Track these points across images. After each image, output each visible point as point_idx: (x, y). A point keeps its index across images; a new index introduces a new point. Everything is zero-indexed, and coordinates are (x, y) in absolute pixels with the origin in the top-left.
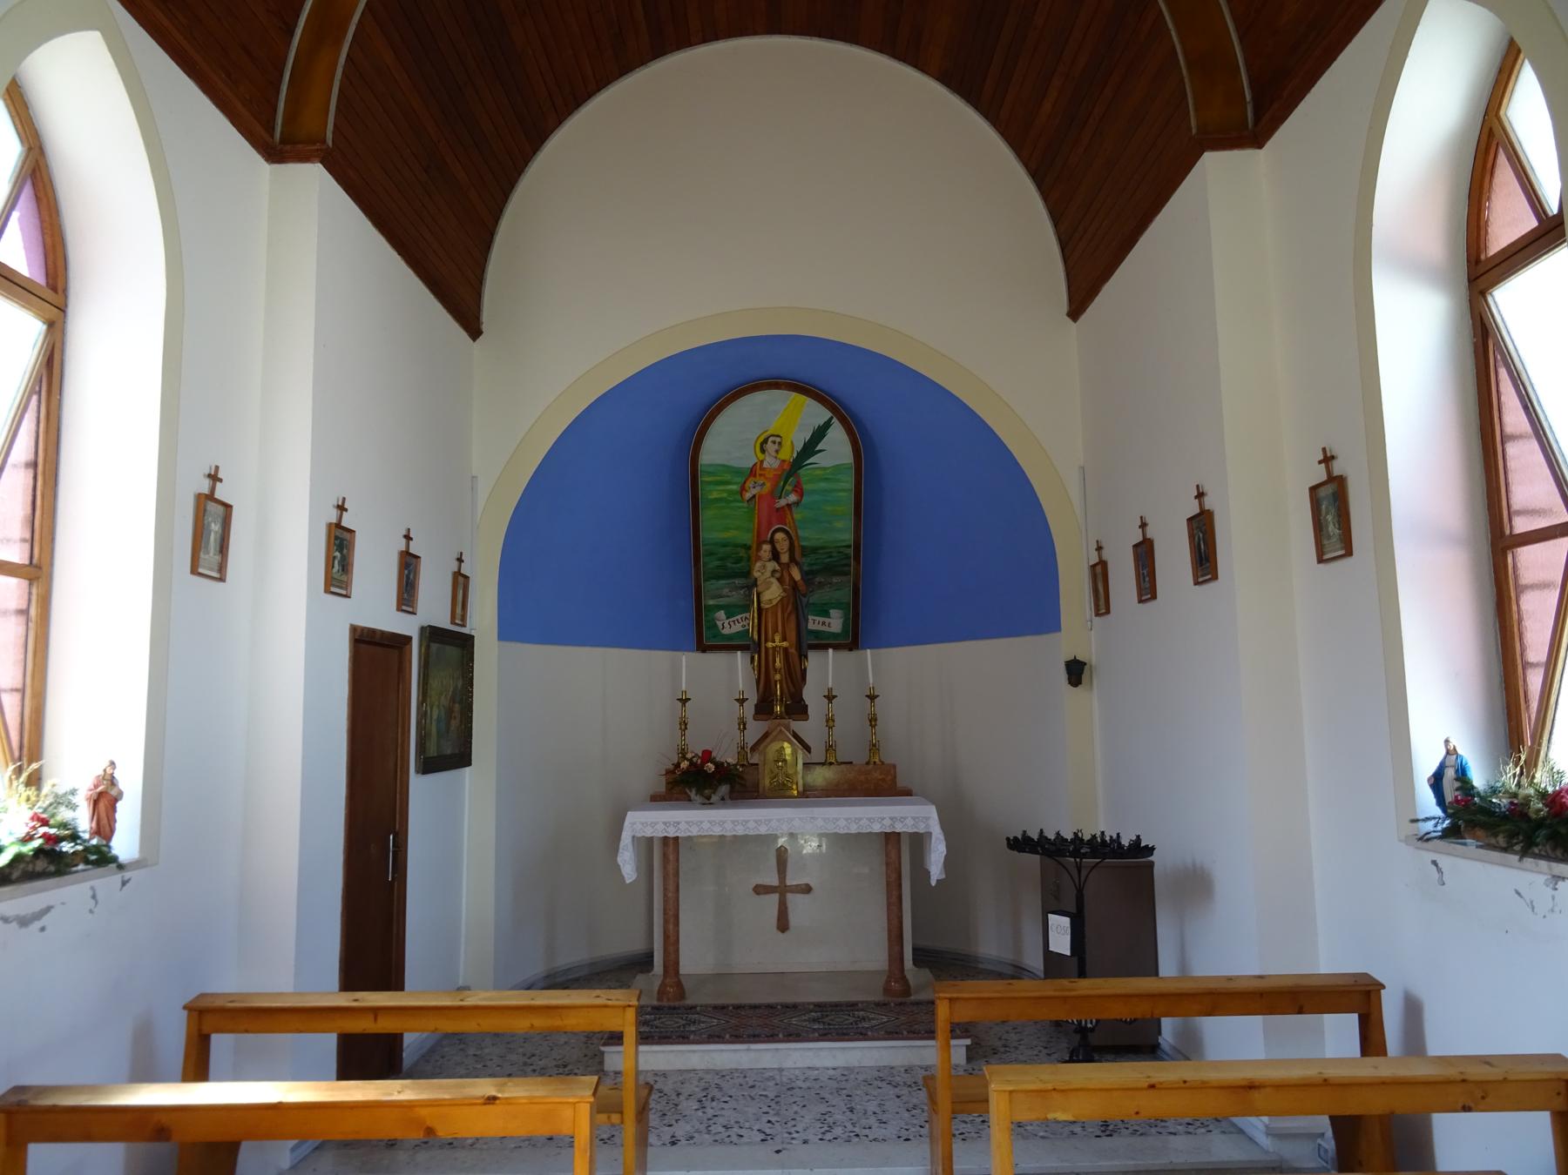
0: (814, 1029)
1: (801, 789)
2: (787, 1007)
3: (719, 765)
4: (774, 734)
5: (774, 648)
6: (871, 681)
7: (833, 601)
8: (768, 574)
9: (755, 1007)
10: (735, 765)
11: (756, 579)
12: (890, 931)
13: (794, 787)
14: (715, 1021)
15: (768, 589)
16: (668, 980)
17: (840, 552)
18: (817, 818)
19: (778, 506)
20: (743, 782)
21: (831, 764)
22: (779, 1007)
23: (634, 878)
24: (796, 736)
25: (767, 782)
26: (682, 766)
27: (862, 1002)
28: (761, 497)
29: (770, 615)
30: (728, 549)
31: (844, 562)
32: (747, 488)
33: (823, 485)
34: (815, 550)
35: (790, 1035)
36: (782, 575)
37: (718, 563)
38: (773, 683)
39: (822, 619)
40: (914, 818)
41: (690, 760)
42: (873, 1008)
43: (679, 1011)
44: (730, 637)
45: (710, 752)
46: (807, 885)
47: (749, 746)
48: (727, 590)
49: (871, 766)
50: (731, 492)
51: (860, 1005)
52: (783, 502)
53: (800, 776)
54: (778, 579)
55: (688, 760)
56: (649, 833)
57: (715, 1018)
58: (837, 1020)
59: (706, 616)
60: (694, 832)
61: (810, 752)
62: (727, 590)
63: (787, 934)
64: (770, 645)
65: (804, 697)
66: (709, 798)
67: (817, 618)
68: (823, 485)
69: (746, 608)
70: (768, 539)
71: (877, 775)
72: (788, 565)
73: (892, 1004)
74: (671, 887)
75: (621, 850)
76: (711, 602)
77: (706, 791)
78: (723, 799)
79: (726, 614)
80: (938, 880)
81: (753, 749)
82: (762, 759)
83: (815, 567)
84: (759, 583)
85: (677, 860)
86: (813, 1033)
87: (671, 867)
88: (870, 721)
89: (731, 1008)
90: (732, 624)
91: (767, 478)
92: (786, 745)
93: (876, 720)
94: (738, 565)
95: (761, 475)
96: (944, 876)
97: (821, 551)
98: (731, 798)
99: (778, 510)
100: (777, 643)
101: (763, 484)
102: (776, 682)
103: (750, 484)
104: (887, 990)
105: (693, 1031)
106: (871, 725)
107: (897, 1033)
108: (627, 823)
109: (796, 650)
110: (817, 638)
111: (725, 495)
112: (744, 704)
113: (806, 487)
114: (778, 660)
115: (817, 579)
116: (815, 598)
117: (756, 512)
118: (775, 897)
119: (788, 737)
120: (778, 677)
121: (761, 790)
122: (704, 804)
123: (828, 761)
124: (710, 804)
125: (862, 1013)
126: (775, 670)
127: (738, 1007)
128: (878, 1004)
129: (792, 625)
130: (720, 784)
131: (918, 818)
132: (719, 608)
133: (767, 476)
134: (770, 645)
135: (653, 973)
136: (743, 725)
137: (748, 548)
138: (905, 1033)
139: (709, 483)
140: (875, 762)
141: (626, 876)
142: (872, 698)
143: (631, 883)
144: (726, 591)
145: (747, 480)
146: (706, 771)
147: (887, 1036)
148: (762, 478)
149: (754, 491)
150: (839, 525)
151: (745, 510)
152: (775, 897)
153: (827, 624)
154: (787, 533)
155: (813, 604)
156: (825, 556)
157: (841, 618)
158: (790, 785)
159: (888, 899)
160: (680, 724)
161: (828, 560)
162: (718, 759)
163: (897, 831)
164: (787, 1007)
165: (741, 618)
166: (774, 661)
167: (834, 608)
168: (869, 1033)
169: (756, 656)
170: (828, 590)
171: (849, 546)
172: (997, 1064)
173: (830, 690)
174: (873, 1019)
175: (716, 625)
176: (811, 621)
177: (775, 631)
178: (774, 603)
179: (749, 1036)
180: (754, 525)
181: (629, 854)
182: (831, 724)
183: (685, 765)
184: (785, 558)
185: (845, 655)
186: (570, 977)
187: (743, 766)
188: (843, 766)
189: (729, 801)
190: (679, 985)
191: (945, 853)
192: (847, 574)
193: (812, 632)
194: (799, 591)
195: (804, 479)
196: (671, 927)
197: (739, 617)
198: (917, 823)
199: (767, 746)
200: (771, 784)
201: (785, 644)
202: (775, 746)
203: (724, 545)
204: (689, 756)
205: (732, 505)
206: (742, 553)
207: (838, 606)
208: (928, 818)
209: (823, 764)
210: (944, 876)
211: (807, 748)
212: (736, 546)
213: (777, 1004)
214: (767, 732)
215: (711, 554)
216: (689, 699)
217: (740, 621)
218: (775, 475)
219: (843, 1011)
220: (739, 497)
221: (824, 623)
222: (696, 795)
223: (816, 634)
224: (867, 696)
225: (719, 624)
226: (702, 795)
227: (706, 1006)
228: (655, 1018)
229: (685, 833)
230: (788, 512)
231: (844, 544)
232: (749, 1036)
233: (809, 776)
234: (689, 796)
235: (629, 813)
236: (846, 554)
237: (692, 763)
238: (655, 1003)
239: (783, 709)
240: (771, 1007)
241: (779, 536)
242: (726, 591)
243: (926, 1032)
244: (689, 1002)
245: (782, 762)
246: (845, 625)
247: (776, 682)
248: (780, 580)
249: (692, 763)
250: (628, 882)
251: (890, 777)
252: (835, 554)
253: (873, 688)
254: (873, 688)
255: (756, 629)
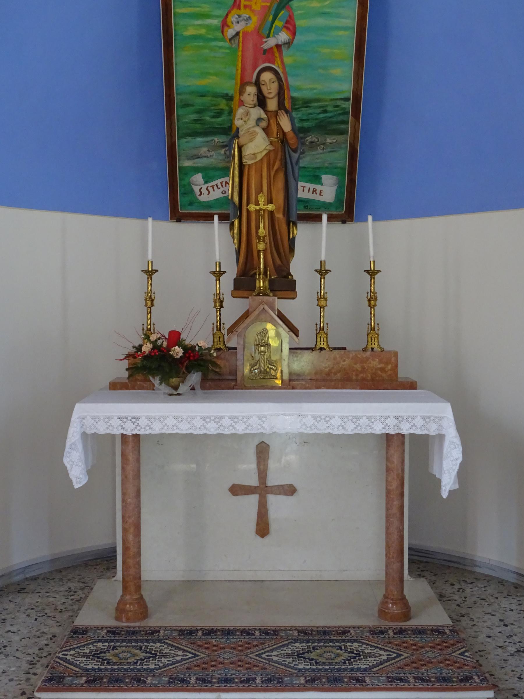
0: (300, 670)
1: (286, 377)
2: (267, 633)
3: (189, 350)
4: (256, 313)
5: (258, 212)
6: (372, 253)
7: (326, 165)
8: (252, 122)
9: (228, 632)
10: (209, 349)
11: (238, 129)
12: (388, 546)
13: (279, 375)
14: (180, 653)
15: (251, 141)
16: (128, 597)
17: (337, 106)
18: (307, 416)
19: (265, 46)
20: (217, 370)
21: (321, 349)
22: (257, 633)
23: (83, 483)
24: (281, 316)
25: (247, 371)
26: (144, 349)
27: (354, 628)
28: (245, 34)
29: (253, 173)
30: (206, 100)
31: (341, 118)
32: (229, 24)
33: (320, 21)
34: (307, 103)
35: (270, 680)
36: (269, 124)
37: (194, 116)
38: (255, 254)
39: (312, 186)
40: (423, 418)
41: (154, 343)
42: (368, 639)
43: (139, 637)
44: (208, 205)
45: (179, 334)
46: (291, 486)
47: (227, 327)
48: (205, 149)
49: (368, 353)
50: (208, 27)
51: (352, 632)
52: (271, 42)
53: (285, 363)
54: (264, 129)
55: (151, 342)
56: (102, 429)
57: (180, 649)
58: (327, 655)
59: (180, 180)
60: (157, 429)
61: (297, 336)
62: (205, 149)
63: (267, 539)
64: (253, 207)
65: (292, 271)
66: (176, 388)
67: (308, 185)
68: (320, 21)
69: (225, 171)
70: (254, 80)
71: (375, 363)
72: (276, 114)
73: (391, 632)
74: (131, 491)
75: (67, 449)
76: (187, 164)
77: (174, 380)
78: (193, 389)
79: (203, 178)
80: (450, 491)
81: (231, 330)
82: (242, 342)
83: (306, 125)
84: (241, 133)
85: (138, 460)
86: (298, 677)
87: (130, 468)
88: (369, 300)
89: (200, 633)
90: (210, 189)
91: (253, 11)
92: (269, 326)
93: (376, 299)
94: (219, 120)
95: (245, 7)
96: (457, 487)
97: (316, 104)
98: (203, 388)
99: (265, 51)
100: (261, 206)
101: (249, 18)
102: (259, 252)
103: (232, 18)
104: (382, 613)
105: (152, 670)
106: (369, 306)
107: (401, 680)
108: (75, 417)
109: (284, 215)
110: (306, 207)
111: (203, 31)
112: (153, 277)
113: (300, 23)
114: (261, 226)
115: (309, 139)
116: (306, 161)
117: (240, 53)
118: (254, 499)
119: (272, 318)
120: (261, 246)
121: (239, 378)
122: (170, 395)
123: (318, 346)
124: (179, 394)
125: (356, 644)
126: (259, 238)
127: (209, 632)
128: (373, 632)
129: (280, 184)
130: (189, 372)
131: (429, 417)
132: (196, 170)
133: (254, 7)
134: (253, 207)
135: (115, 578)
136: (219, 303)
137: (229, 98)
138: (412, 680)
139: (185, 15)
140: (372, 349)
141: (74, 480)
142: (372, 273)
143: (79, 488)
144: (204, 150)
145: (229, 12)
146: (172, 356)
147: (389, 685)
148: (248, 10)
149: (238, 28)
150: (337, 72)
151: (227, 51)
152: (254, 499)
153: (318, 192)
154: (276, 73)
155: (304, 168)
156: (319, 111)
157: (334, 185)
158: (273, 373)
159: (387, 509)
160: (146, 300)
161: (322, 116)
162: (187, 342)
163: (402, 432)
164: (267, 633)
165: (221, 183)
166: (258, 228)
167: (326, 173)
168: (367, 679)
169: (236, 222)
170: (321, 151)
171: (347, 99)
172: (187, 107)
173: (323, 263)
174: (370, 655)
175: (192, 191)
176: (300, 189)
177: (260, 190)
178: (259, 158)
179: (220, 681)
180: (237, 70)
181: (78, 454)
182: (323, 303)
183: (147, 348)
184: (272, 105)
185: (339, 228)
186: (28, 576)
187: (219, 349)
188: (336, 352)
189: (199, 391)
190: (141, 602)
191: (460, 460)
192: (343, 132)
193: (300, 201)
194: (288, 144)
195: (296, 13)
196: (131, 537)
197: (218, 182)
198: (427, 423)
199: (246, 328)
200: (251, 372)
201: (271, 207)
202: (257, 328)
203: (203, 95)
204: (153, 338)
205: (214, 43)
206: (223, 104)
207: (331, 170)
208: (441, 418)
209: (312, 349)
210: (457, 487)
211: (294, 330)
212: (216, 95)
213: (255, 628)
214: (248, 311)
215: (187, 105)
216: (157, 271)
217: (220, 186)
218: (262, 7)
219: (332, 641)
220: (219, 34)
221: (314, 191)
222: (161, 383)
223: (306, 203)
224: (316, 271)
225: (196, 189)
226: (168, 385)
227: (172, 629)
228: (109, 646)
229: (146, 430)
230: (277, 54)
231: (342, 96)
232: (220, 681)
233: (296, 364)
234: (154, 385)
235: (78, 406)
236: (344, 109)
237: (156, 347)
238: (112, 623)
239: (267, 284)
240: (248, 633)
241: (267, 76)
242: (204, 150)
243: (438, 679)
244: (152, 622)
245: (264, 346)
246: (338, 194)
247: (259, 252)
248: (266, 130)
249: (156, 347)
250: (76, 487)
251: (390, 367)
252: (329, 109)
253: (374, 262)
254: (374, 262)
255: (236, 190)
